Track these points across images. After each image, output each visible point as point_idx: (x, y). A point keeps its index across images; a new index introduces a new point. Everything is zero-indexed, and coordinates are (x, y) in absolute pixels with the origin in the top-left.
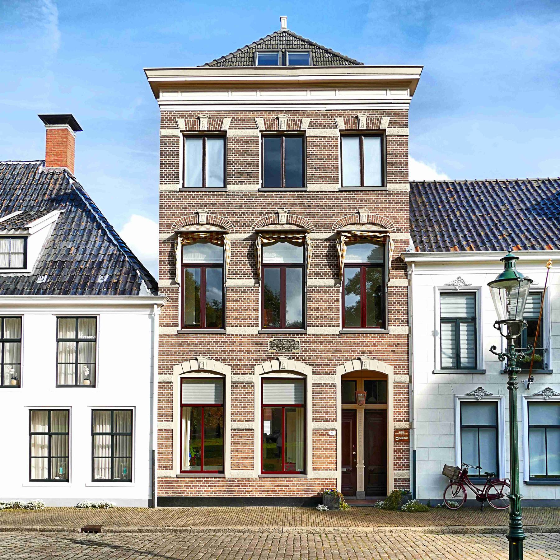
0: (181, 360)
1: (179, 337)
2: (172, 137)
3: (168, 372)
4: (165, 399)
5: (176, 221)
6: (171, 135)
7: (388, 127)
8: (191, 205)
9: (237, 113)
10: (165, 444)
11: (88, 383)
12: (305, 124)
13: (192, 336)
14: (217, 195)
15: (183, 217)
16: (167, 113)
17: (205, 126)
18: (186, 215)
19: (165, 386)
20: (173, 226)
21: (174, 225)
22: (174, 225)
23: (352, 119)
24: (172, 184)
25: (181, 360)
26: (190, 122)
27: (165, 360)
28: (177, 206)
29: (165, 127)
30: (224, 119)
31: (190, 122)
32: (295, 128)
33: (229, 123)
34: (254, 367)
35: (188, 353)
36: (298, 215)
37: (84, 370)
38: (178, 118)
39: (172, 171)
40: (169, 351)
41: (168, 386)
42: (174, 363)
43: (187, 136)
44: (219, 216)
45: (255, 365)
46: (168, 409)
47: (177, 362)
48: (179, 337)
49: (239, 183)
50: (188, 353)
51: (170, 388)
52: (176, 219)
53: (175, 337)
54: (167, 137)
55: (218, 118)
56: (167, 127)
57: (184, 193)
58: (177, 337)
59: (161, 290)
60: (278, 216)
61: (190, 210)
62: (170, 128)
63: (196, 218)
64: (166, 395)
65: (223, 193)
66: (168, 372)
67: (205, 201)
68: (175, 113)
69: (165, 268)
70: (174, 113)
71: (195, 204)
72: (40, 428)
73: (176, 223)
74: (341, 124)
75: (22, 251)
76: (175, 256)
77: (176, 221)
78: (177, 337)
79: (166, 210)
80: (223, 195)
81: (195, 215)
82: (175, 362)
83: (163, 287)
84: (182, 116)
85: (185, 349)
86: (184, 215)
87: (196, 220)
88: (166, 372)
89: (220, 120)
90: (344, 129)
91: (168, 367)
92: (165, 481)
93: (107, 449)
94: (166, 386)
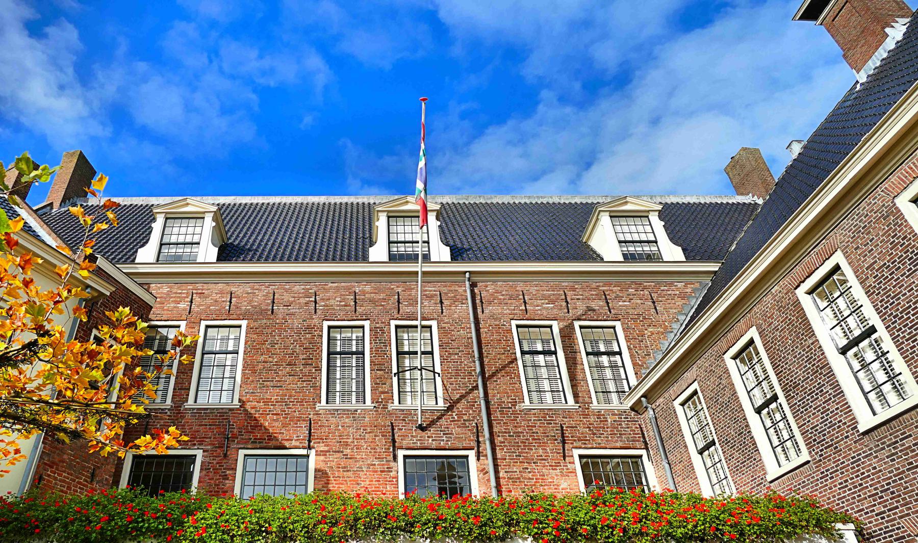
32: (567, 437)
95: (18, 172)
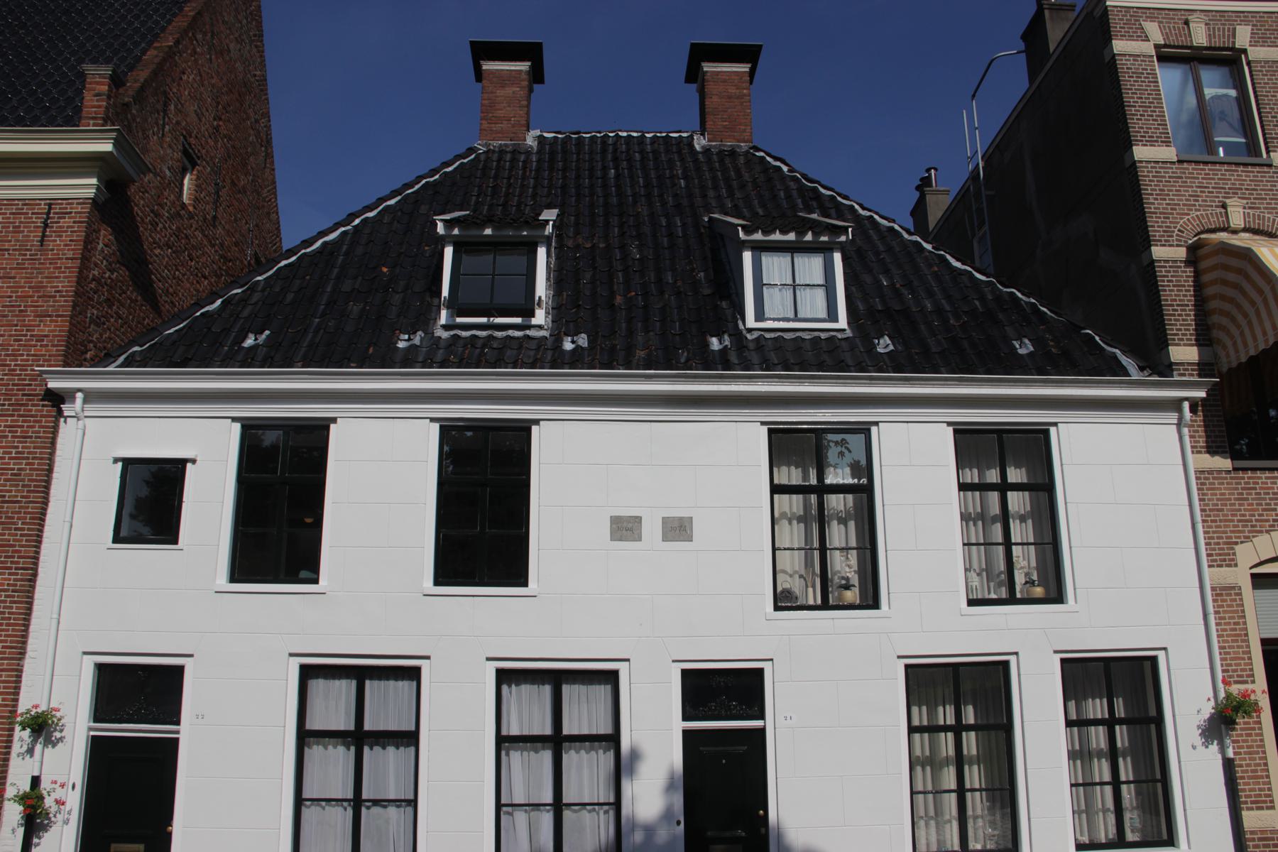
0: (1249, 532)
1: (1237, 478)
2: (1138, 56)
3: (1225, 560)
4: (1227, 627)
5: (1182, 221)
6: (1137, 52)
7: (1250, 46)
8: (1206, 190)
9: (1260, 17)
10: (1244, 741)
11: (1039, 591)
12: (1243, 37)
13: (1263, 476)
14: (1253, 172)
15: (1194, 214)
16: (1121, 11)
17: (1200, 36)
18: (1199, 210)
19: (1221, 595)
20: (1176, 232)
21: (1179, 230)
22: (1179, 231)
23: (1174, 27)
24: (1159, 146)
25: (1249, 532)
26: (1170, 30)
27: (1214, 532)
28: (1176, 191)
29: (1121, 36)
30: (1238, 27)
31: (1170, 30)
33: (1249, 35)
34: (1233, 549)
35: (1262, 515)
36: (1264, 213)
37: (844, 565)
38: (1143, 21)
39: (1153, 120)
40: (1218, 510)
41: (1231, 595)
42: (1234, 540)
43: (1166, 56)
44: (1267, 215)
45: (1236, 543)
46: (1239, 653)
47: (1239, 537)
48: (1237, 478)
49: (1148, 144)
50: (1262, 515)
51: (1235, 600)
52: (1181, 219)
53: (1226, 478)
54: (1130, 55)
55: (1224, 24)
56: (1125, 36)
57: (1185, 165)
58: (1231, 478)
59: (1179, 369)
60: (1226, 213)
61: (1206, 201)
62: (1131, 38)
63: (1222, 217)
64: (1230, 618)
65: (1266, 169)
66: (1225, 560)
67: (1233, 184)
68: (1135, 12)
69: (1178, 320)
70: (1134, 12)
71: (1213, 188)
72: (1096, 708)
73: (1181, 226)
74: (1155, 33)
75: (821, 281)
76: (170, 834)
77: (1182, 221)
78: (1231, 478)
79: (1156, 199)
80: (1265, 172)
81: (1219, 210)
82: (1236, 537)
83: (1182, 364)
84: (1152, 19)
85: (1252, 504)
86: (1196, 210)
87: (1223, 221)
88: (1221, 560)
89: (1229, 28)
90: (1163, 42)
91: (1223, 549)
92: (1260, 839)
93: (975, 768)
94: (1227, 594)
95: (1250, 27)
